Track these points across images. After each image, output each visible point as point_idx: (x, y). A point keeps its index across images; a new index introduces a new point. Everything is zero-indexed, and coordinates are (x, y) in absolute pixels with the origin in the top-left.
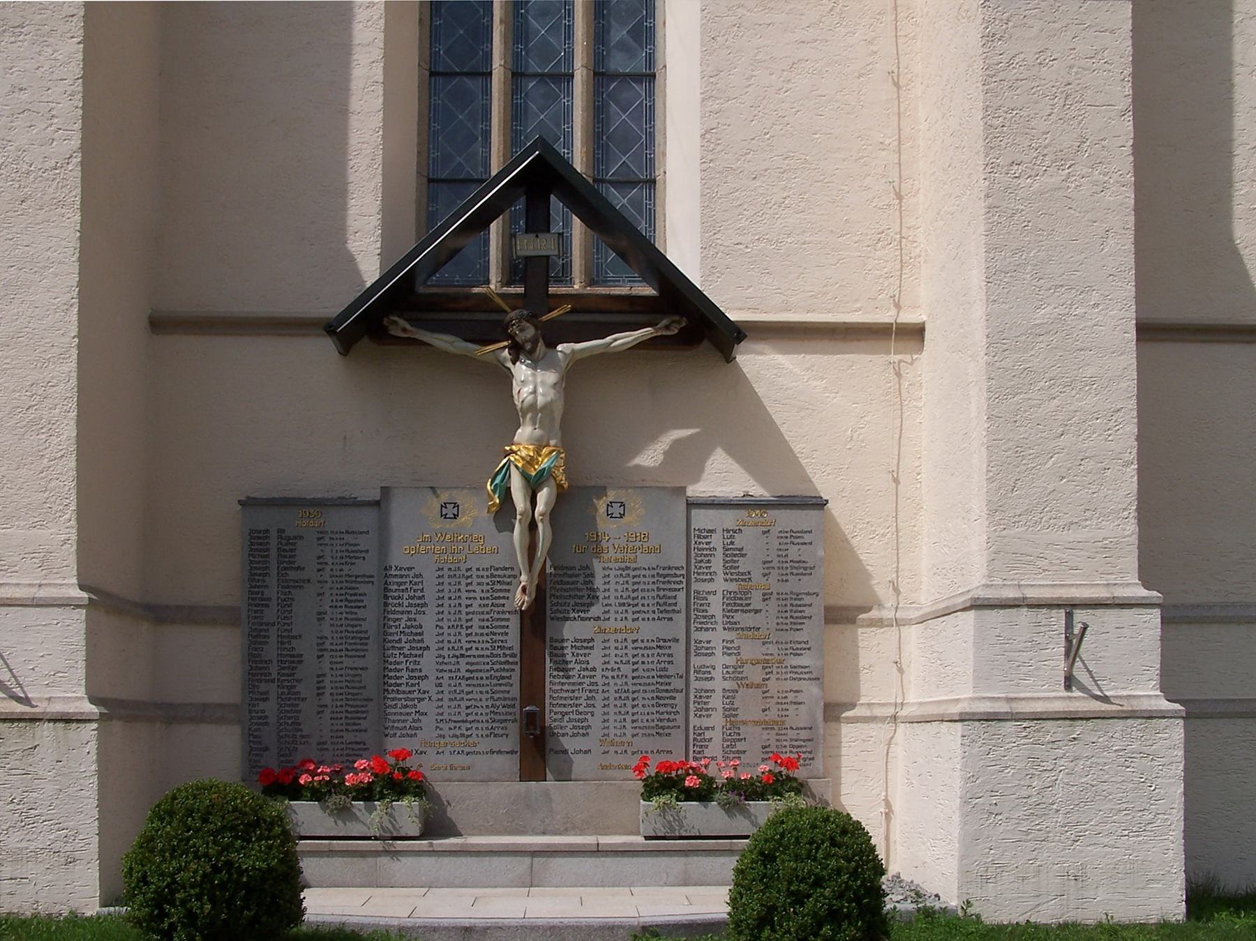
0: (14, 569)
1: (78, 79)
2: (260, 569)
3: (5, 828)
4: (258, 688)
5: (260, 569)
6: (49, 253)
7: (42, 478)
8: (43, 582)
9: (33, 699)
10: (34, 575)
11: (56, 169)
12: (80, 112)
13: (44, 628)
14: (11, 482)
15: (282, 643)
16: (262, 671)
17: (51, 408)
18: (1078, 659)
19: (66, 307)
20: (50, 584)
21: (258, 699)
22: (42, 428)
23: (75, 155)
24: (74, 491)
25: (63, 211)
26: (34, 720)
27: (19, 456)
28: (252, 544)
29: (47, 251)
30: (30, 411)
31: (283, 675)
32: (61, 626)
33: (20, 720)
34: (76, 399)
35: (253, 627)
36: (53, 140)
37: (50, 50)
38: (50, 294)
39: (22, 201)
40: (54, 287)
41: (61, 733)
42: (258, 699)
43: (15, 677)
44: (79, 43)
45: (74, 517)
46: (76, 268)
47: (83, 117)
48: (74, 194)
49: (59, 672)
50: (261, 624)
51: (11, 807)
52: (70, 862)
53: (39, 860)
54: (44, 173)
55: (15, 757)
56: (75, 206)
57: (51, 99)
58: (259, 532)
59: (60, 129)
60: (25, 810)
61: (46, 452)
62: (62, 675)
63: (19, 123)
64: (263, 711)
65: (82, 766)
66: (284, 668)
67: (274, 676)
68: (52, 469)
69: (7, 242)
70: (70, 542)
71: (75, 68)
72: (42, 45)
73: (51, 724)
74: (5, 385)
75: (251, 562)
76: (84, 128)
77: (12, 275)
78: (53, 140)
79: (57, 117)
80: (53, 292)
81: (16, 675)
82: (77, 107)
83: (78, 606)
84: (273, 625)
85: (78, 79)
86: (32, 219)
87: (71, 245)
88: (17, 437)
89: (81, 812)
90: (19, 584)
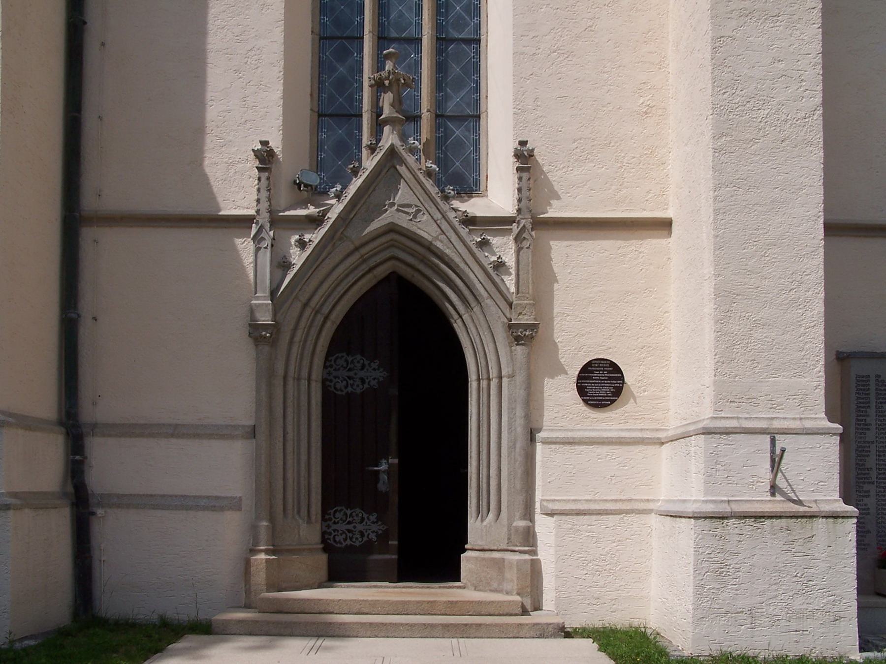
0: (781, 407)
1: (819, 54)
2: (863, 403)
3: (791, 594)
4: (862, 488)
5: (863, 403)
6: (802, 179)
7: (800, 341)
8: (802, 416)
9: (805, 501)
10: (796, 411)
11: (805, 119)
12: (821, 78)
13: (810, 450)
14: (779, 344)
15: (880, 456)
16: (865, 476)
17: (806, 291)
18: (779, 471)
19: (815, 218)
20: (808, 418)
21: (863, 496)
22: (799, 305)
23: (818, 108)
24: (823, 351)
25: (811, 148)
26: (812, 516)
27: (784, 326)
28: (858, 385)
29: (801, 177)
30: (791, 293)
31: (880, 478)
32: (823, 448)
33: (802, 517)
34: (823, 285)
35: (859, 445)
36: (803, 97)
37: (798, 33)
38: (803, 208)
39: (782, 141)
40: (806, 203)
41: (831, 526)
42: (863, 496)
43: (790, 485)
44: (819, 28)
45: (823, 369)
46: (821, 191)
47: (823, 81)
48: (818, 137)
49: (821, 481)
50: (865, 442)
51: (795, 579)
52: (837, 620)
53: (815, 618)
54: (797, 121)
55: (799, 543)
56: (820, 146)
57: (800, 68)
58: (863, 377)
59: (807, 90)
60: (805, 581)
61: (802, 323)
62: (823, 483)
63: (778, 85)
64: (866, 505)
65: (846, 550)
66: (880, 474)
67: (874, 479)
68: (807, 335)
69: (773, 170)
70: (820, 387)
71: (817, 46)
72: (792, 29)
73: (824, 520)
74: (774, 273)
75: (858, 398)
76: (824, 91)
77: (777, 194)
78: (803, 97)
79: (805, 81)
80: (805, 207)
81: (791, 484)
82: (818, 74)
83: (834, 434)
84: (873, 442)
85: (819, 54)
86: (790, 154)
87: (817, 173)
88: (783, 311)
89: (845, 583)
90: (786, 418)
